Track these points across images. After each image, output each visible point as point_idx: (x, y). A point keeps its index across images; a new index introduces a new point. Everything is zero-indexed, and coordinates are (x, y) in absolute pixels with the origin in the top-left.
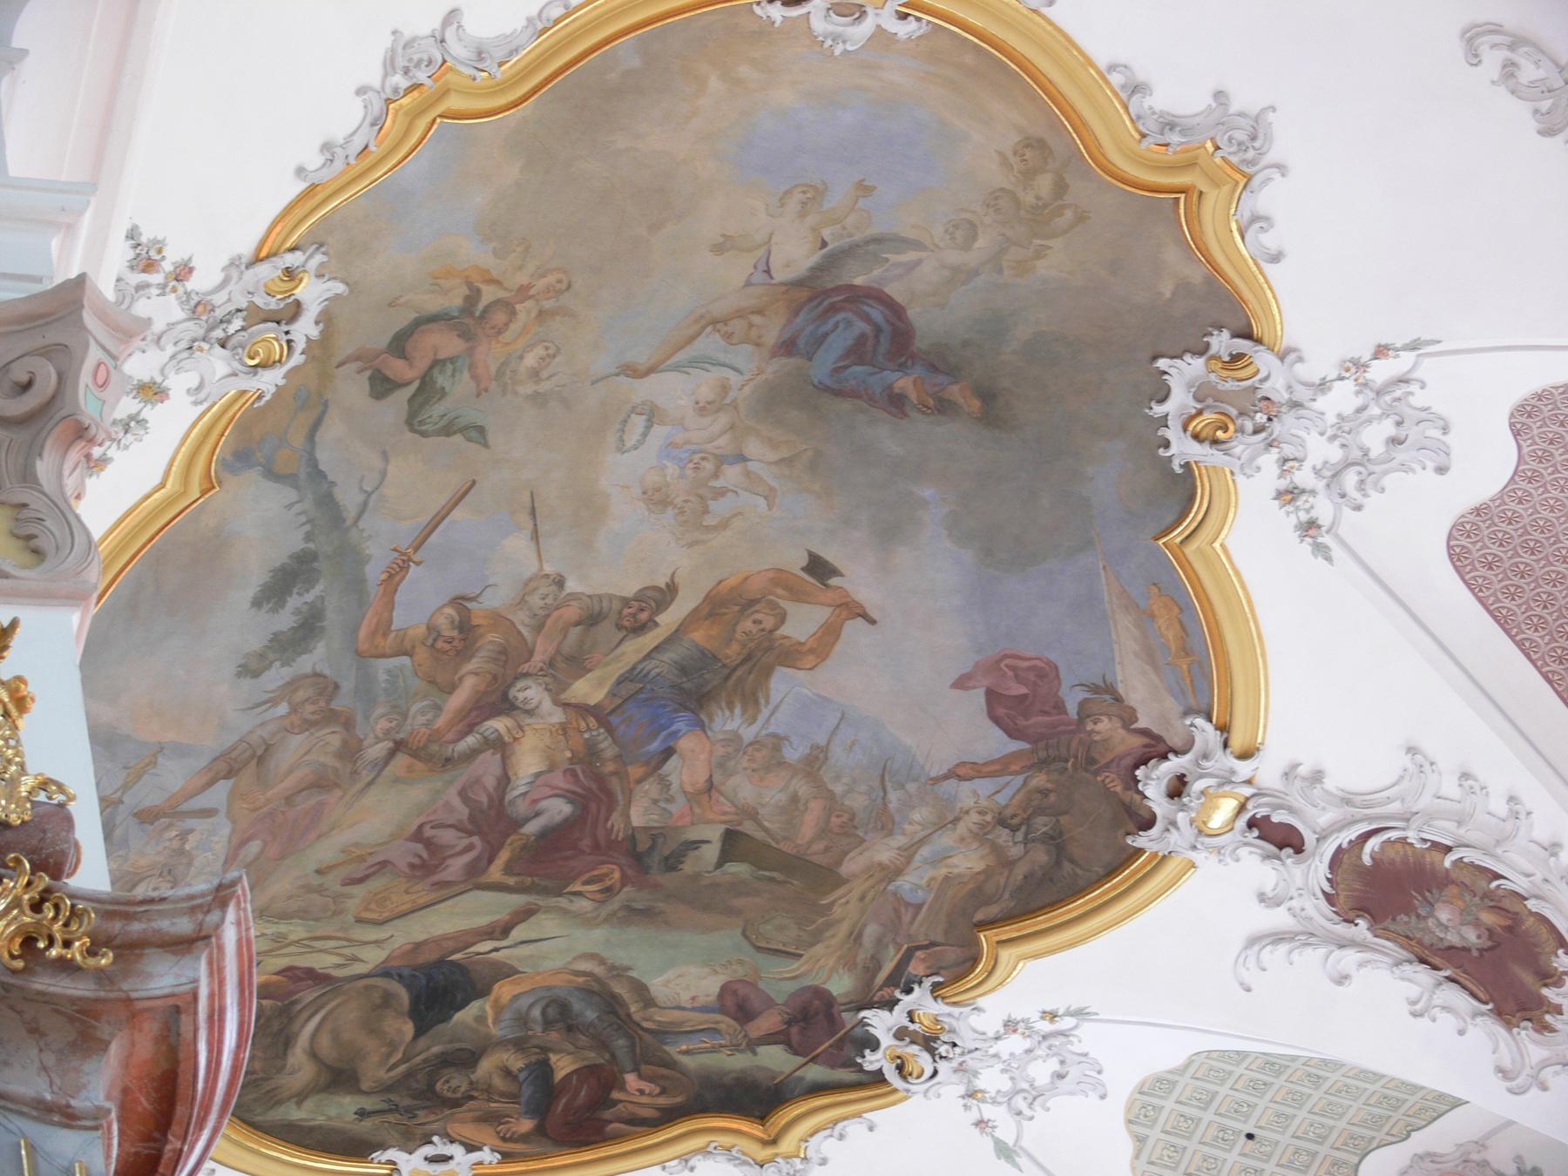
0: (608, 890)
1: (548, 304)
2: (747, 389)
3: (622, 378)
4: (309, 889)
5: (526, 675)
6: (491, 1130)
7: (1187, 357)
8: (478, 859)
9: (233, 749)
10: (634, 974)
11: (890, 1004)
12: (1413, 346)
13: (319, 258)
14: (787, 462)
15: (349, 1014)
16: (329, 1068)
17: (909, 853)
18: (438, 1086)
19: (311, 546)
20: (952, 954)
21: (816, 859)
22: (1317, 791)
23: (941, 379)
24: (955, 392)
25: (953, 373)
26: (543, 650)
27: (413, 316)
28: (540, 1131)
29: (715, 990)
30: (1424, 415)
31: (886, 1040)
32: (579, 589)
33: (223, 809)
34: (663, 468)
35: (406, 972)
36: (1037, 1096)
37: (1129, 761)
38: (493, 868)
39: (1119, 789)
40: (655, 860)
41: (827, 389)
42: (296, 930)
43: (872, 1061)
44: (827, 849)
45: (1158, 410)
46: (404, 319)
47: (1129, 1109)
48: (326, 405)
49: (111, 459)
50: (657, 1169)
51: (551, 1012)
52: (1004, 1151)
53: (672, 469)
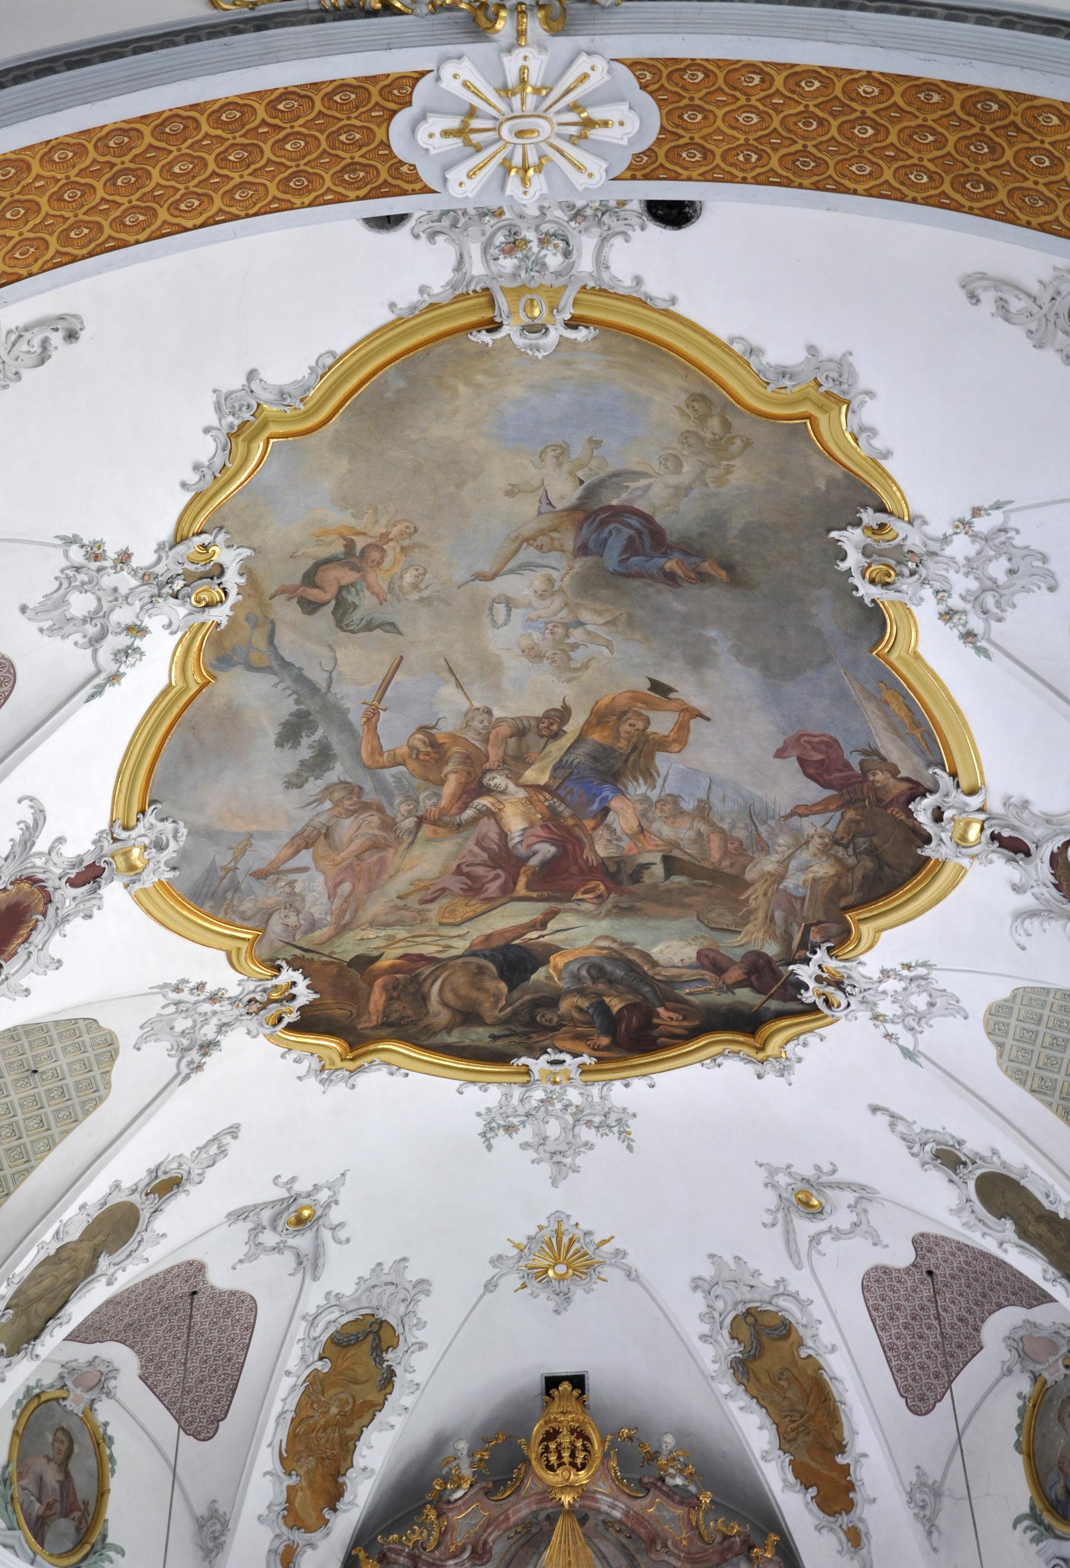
0: (599, 897)
1: (406, 543)
2: (567, 579)
3: (477, 582)
4: (397, 908)
5: (490, 770)
6: (583, 1044)
7: (849, 528)
8: (506, 882)
9: (303, 831)
10: (638, 947)
11: (807, 961)
12: (997, 506)
13: (222, 537)
14: (612, 623)
15: (460, 979)
16: (460, 1012)
17: (785, 862)
18: (538, 1019)
19: (302, 707)
20: (834, 928)
21: (727, 870)
22: (1025, 815)
23: (694, 559)
24: (706, 566)
25: (702, 554)
26: (495, 754)
27: (311, 562)
28: (615, 1044)
29: (694, 955)
30: (1026, 552)
31: (812, 984)
32: (503, 715)
33: (312, 865)
34: (530, 635)
35: (487, 953)
36: (920, 1017)
37: (903, 799)
38: (518, 888)
39: (903, 817)
40: (623, 877)
41: (620, 574)
42: (401, 933)
43: (808, 997)
44: (732, 865)
45: (843, 566)
46: (307, 564)
47: (986, 1026)
48: (273, 623)
49: (124, 674)
50: (699, 1065)
51: (593, 972)
52: (908, 1054)
53: (536, 636)
